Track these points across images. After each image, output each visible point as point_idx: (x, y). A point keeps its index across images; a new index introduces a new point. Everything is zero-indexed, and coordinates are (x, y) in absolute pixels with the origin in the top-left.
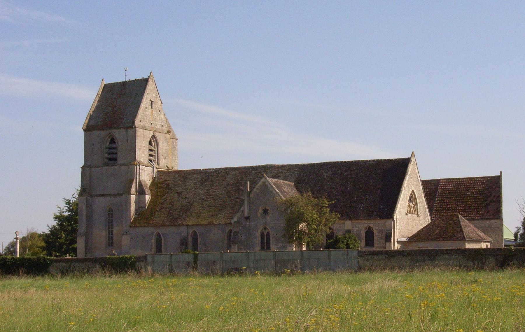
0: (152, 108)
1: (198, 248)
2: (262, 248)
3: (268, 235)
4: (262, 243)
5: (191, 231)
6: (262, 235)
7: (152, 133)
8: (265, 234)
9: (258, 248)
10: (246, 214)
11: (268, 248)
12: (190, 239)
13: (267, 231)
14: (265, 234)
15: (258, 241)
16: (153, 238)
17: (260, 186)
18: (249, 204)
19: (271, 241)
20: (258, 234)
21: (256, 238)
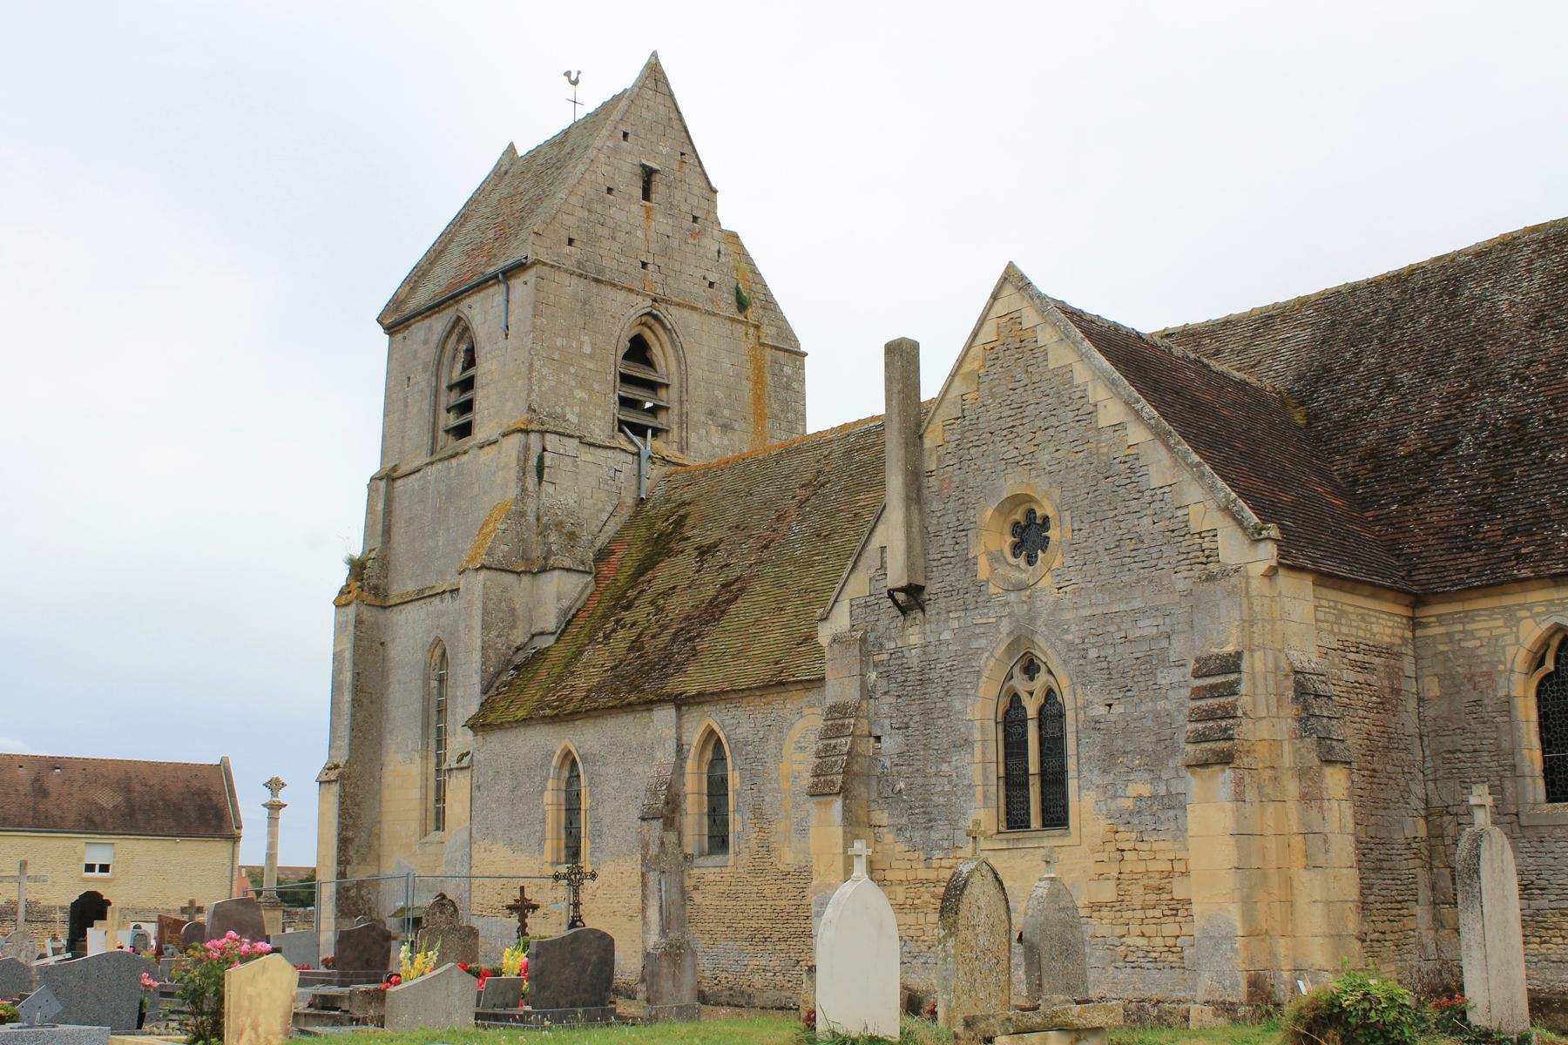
0: (646, 195)
1: (1066, 819)
2: (1015, 819)
3: (1052, 713)
4: (1014, 782)
5: (694, 737)
6: (1012, 720)
7: (644, 304)
8: (1032, 708)
9: (983, 811)
10: (897, 576)
11: (1056, 817)
12: (693, 785)
13: (1042, 678)
14: (1032, 708)
15: (977, 768)
16: (550, 784)
17: (1134, 467)
18: (915, 494)
19: (1071, 764)
20: (978, 713)
21: (967, 743)
